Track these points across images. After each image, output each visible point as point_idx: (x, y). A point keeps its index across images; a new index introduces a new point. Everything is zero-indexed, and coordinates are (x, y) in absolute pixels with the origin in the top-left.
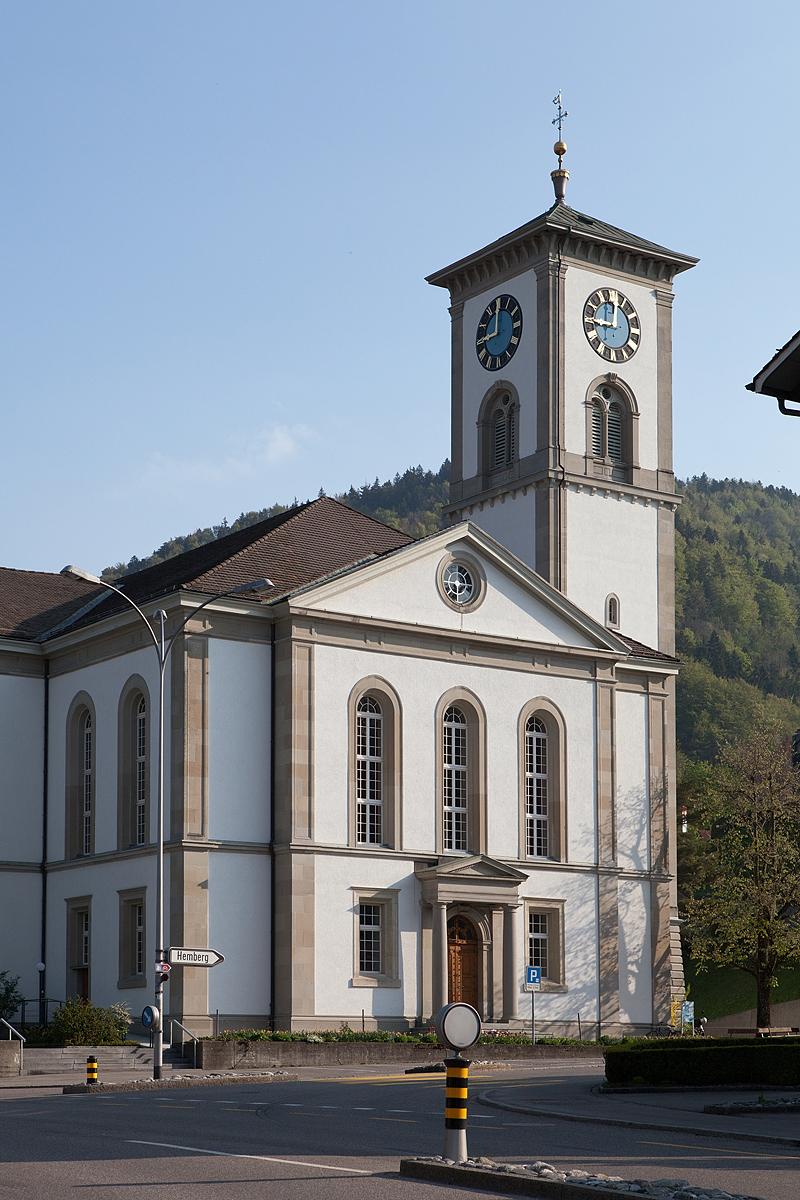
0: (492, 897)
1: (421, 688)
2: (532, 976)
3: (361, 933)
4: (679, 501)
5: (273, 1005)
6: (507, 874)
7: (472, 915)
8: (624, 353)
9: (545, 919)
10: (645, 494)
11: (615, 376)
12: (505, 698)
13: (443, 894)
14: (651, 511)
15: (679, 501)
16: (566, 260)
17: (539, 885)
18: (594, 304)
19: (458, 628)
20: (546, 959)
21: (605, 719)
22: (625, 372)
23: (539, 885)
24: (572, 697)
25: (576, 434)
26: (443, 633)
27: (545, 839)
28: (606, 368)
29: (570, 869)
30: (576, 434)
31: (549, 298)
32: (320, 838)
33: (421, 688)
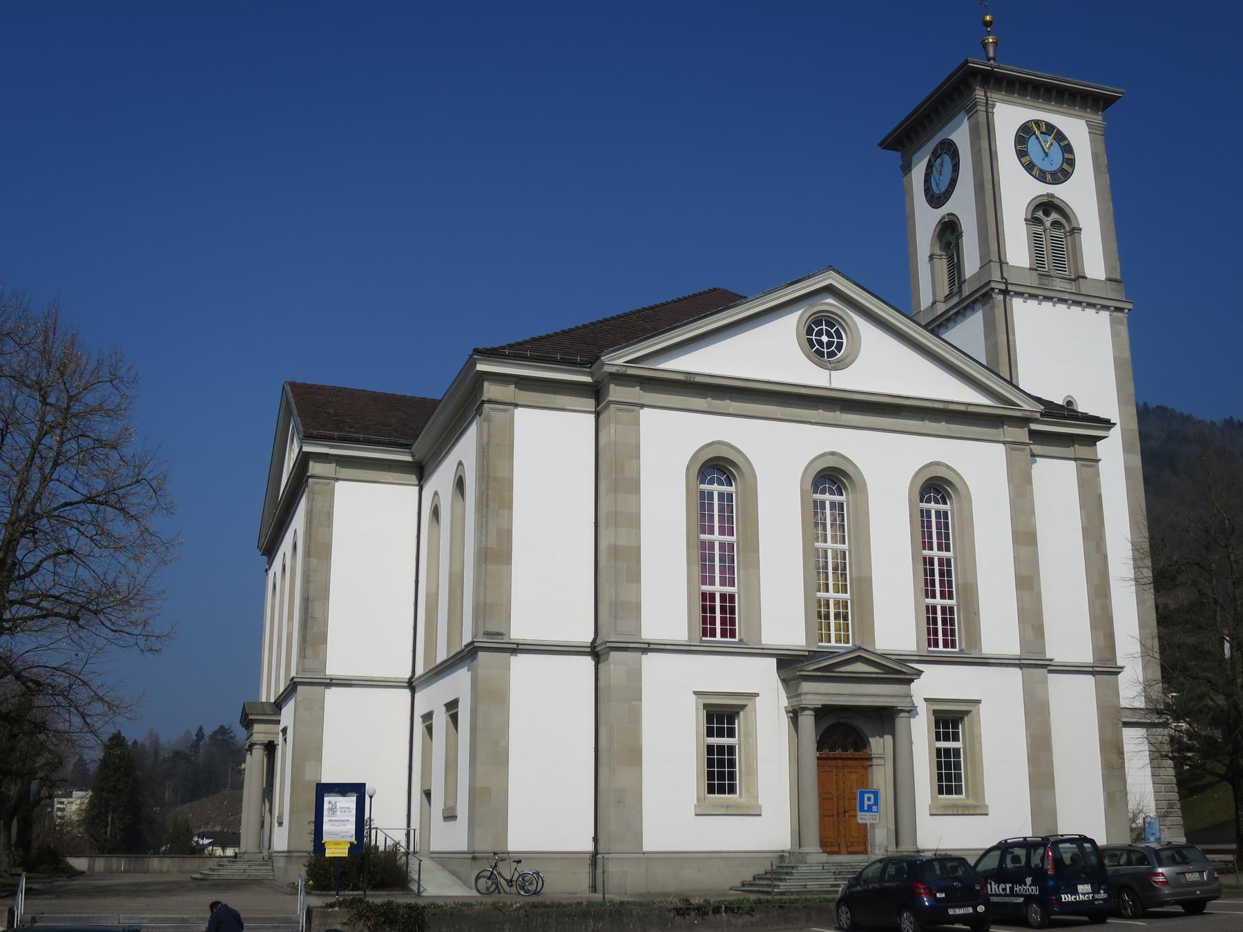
0: (875, 699)
1: (779, 455)
2: (866, 803)
3: (710, 749)
4: (1130, 306)
5: (596, 839)
6: (899, 672)
7: (862, 725)
8: (1062, 175)
9: (949, 721)
10: (1093, 301)
11: (1052, 196)
12: (888, 464)
13: (809, 696)
14: (1105, 315)
15: (1130, 306)
16: (993, 96)
17: (937, 683)
18: (1025, 133)
19: (828, 385)
20: (950, 774)
21: (1021, 486)
22: (1060, 191)
23: (937, 683)
24: (980, 464)
25: (1018, 250)
26: (803, 391)
27: (947, 630)
28: (1042, 189)
29: (985, 662)
30: (1018, 250)
31: (984, 134)
32: (649, 632)
33: (779, 455)
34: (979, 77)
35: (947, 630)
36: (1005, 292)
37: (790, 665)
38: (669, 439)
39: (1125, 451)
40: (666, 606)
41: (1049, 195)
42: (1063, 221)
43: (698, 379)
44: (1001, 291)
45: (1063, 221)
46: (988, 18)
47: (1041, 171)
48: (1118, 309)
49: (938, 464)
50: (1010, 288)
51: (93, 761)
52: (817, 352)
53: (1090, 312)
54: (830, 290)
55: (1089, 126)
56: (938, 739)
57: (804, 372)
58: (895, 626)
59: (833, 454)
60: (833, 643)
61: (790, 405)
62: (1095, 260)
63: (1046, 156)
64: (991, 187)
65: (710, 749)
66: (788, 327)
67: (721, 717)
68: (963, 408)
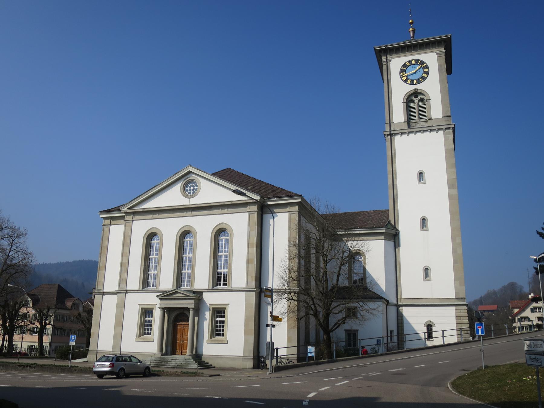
10: (433, 128)
20: (218, 330)
23: (211, 299)
26: (177, 207)
27: (219, 280)
28: (411, 88)
34: (383, 52)
35: (219, 280)
36: (390, 134)
37: (166, 296)
38: (141, 227)
39: (448, 188)
40: (134, 280)
41: (416, 89)
42: (422, 97)
43: (146, 210)
44: (388, 135)
45: (422, 97)
46: (410, 21)
47: (417, 80)
48: (446, 129)
49: (222, 223)
50: (392, 132)
51: (284, 313)
52: (196, 190)
53: (434, 133)
54: (190, 172)
55: (437, 54)
56: (152, 321)
57: (181, 201)
58: (201, 279)
59: (187, 226)
60: (186, 287)
61: (176, 212)
62: (437, 109)
63: (417, 73)
64: (387, 94)
65: (224, 317)
66: (178, 187)
67: (147, 312)
68: (230, 203)
